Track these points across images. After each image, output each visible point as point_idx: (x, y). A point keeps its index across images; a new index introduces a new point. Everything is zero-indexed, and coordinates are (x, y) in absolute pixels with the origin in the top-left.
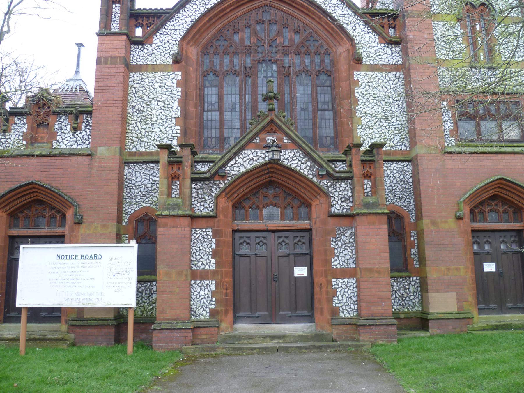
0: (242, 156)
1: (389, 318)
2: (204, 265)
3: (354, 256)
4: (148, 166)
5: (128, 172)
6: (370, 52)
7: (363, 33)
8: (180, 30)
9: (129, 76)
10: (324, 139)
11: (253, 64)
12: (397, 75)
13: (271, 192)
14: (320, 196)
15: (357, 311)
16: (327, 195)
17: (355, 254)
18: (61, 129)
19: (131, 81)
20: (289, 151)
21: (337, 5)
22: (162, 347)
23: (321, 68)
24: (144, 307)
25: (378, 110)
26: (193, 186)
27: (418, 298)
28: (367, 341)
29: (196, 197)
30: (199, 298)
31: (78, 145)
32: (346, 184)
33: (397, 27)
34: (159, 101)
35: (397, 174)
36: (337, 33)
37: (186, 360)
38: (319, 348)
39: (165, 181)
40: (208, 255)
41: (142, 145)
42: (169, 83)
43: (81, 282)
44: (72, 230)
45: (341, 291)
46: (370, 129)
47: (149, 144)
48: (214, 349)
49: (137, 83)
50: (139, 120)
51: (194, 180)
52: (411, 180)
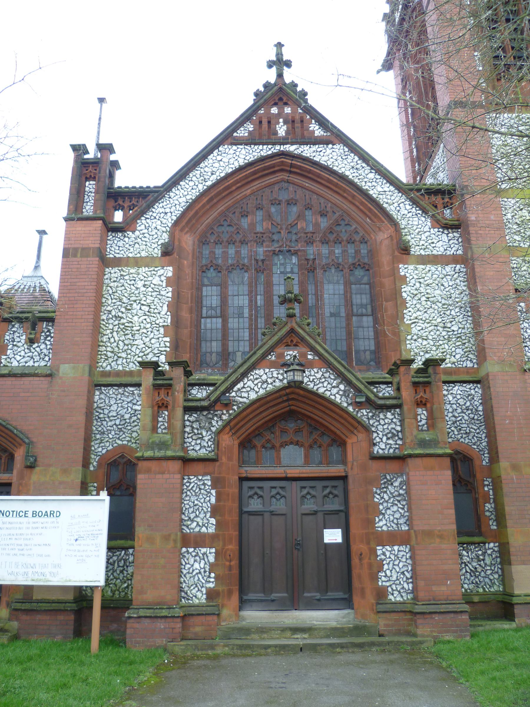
0: (252, 377)
1: (458, 602)
2: (200, 526)
3: (407, 514)
4: (127, 390)
5: (100, 399)
6: (420, 239)
7: (410, 214)
8: (172, 213)
9: (105, 272)
10: (362, 353)
11: (267, 256)
12: (457, 268)
13: (291, 426)
14: (358, 431)
15: (413, 592)
16: (367, 430)
17: (407, 511)
18: (13, 341)
19: (107, 279)
20: (315, 370)
21: (374, 180)
22: (138, 643)
23: (356, 260)
24: (116, 586)
25: (433, 315)
26: (186, 417)
27: (497, 572)
28: (428, 636)
29: (190, 433)
30: (192, 573)
31: (34, 362)
32: (393, 414)
34: (143, 305)
35: (462, 400)
37: (172, 663)
38: (360, 646)
39: (149, 411)
40: (205, 513)
41: (119, 362)
42: (156, 281)
43: (31, 549)
44: (21, 477)
47: (128, 360)
48: (212, 647)
49: (114, 281)
50: (116, 329)
51: (188, 410)
52: (480, 408)
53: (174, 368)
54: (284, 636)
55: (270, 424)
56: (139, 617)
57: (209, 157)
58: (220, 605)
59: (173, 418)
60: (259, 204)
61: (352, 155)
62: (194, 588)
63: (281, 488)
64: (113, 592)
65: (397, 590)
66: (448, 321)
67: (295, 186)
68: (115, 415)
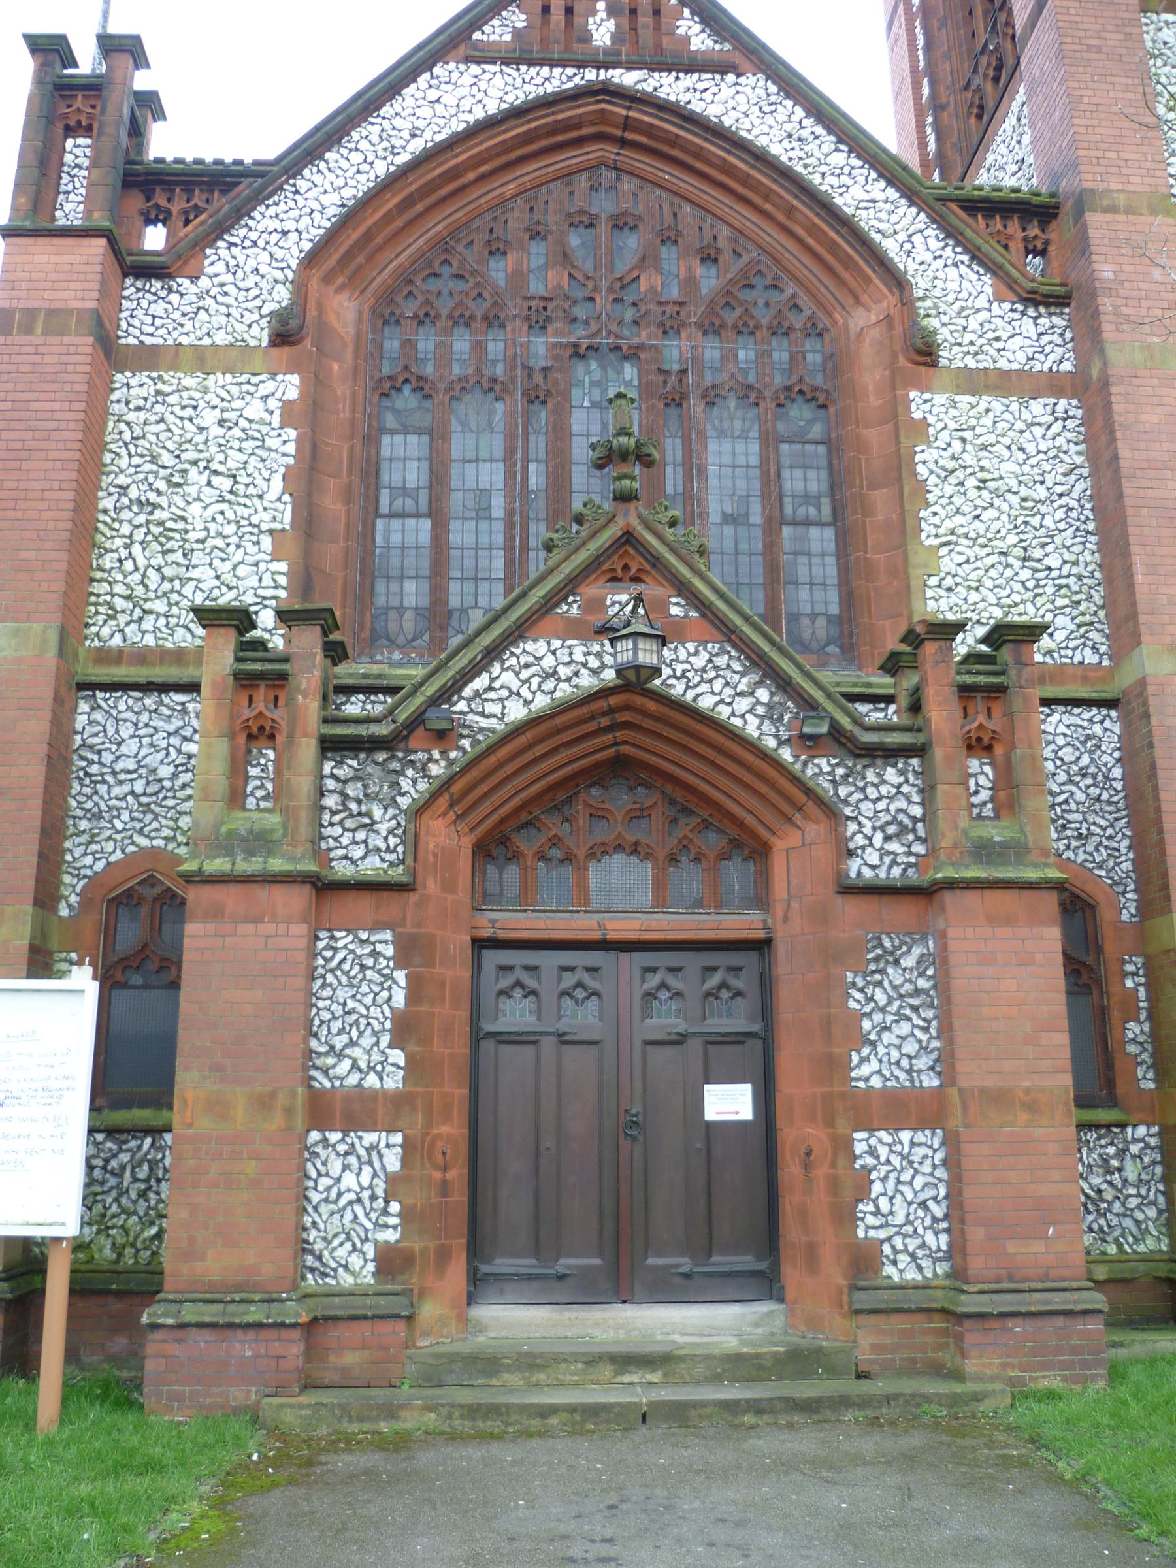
0: (514, 661)
1: (1075, 1285)
2: (360, 1070)
3: (936, 1044)
4: (166, 700)
5: (90, 723)
6: (965, 328)
7: (939, 263)
8: (300, 233)
9: (112, 382)
10: (806, 622)
11: (556, 358)
14: (807, 817)
15: (949, 1256)
16: (830, 811)
17: (938, 1037)
19: (118, 401)
20: (691, 646)
21: (847, 170)
22: (179, 1398)
23: (795, 378)
24: (127, 1232)
25: (996, 525)
26: (328, 767)
27: (1154, 1203)
28: (993, 1379)
30: (336, 1202)
32: (902, 773)
33: (1051, 248)
34: (215, 472)
35: (1069, 749)
36: (848, 263)
38: (810, 1407)
39: (222, 747)
40: (375, 1034)
41: (148, 624)
42: (255, 410)
45: (886, 1177)
46: (969, 588)
47: (173, 621)
48: (391, 1412)
49: (138, 409)
51: (331, 746)
52: (1117, 772)
53: (294, 629)
54: (594, 1377)
55: (561, 796)
56: (183, 1326)
57: (405, 91)
58: (416, 1291)
59: (289, 768)
60: (538, 223)
61: (789, 103)
62: (341, 1244)
63: (589, 969)
64: (119, 1250)
65: (906, 1250)
66: (1035, 542)
67: (634, 180)
68: (132, 767)
